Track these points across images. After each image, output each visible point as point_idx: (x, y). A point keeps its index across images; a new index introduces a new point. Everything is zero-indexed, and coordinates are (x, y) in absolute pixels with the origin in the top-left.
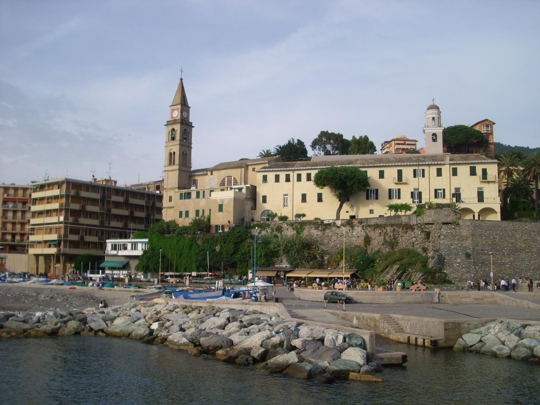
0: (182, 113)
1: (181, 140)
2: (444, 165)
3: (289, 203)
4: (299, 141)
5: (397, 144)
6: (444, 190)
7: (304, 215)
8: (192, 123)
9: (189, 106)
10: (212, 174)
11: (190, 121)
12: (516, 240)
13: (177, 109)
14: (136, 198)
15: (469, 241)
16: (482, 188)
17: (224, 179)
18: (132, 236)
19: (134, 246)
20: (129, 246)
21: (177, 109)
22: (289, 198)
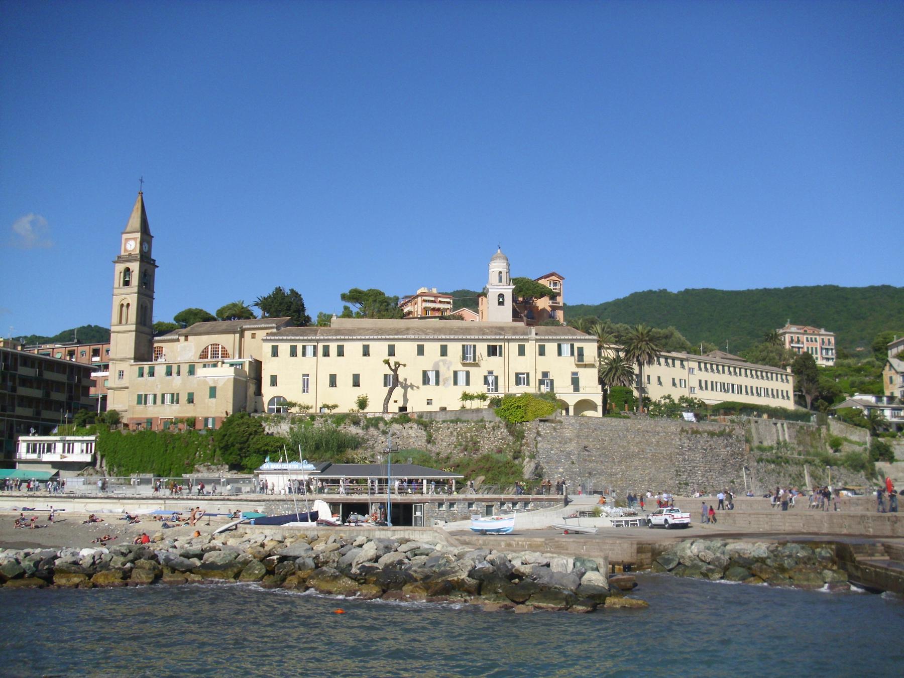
0: (141, 244)
1: (140, 286)
2: (527, 340)
3: (312, 386)
4: (292, 291)
5: (425, 301)
6: (528, 374)
7: (335, 407)
8: (154, 261)
9: (152, 234)
10: (186, 340)
11: (153, 257)
12: (628, 443)
13: (135, 239)
14: (52, 370)
15: (574, 444)
16: (576, 373)
17: (207, 348)
18: (33, 430)
19: (69, 447)
20: (59, 446)
21: (135, 239)
22: (312, 379)
